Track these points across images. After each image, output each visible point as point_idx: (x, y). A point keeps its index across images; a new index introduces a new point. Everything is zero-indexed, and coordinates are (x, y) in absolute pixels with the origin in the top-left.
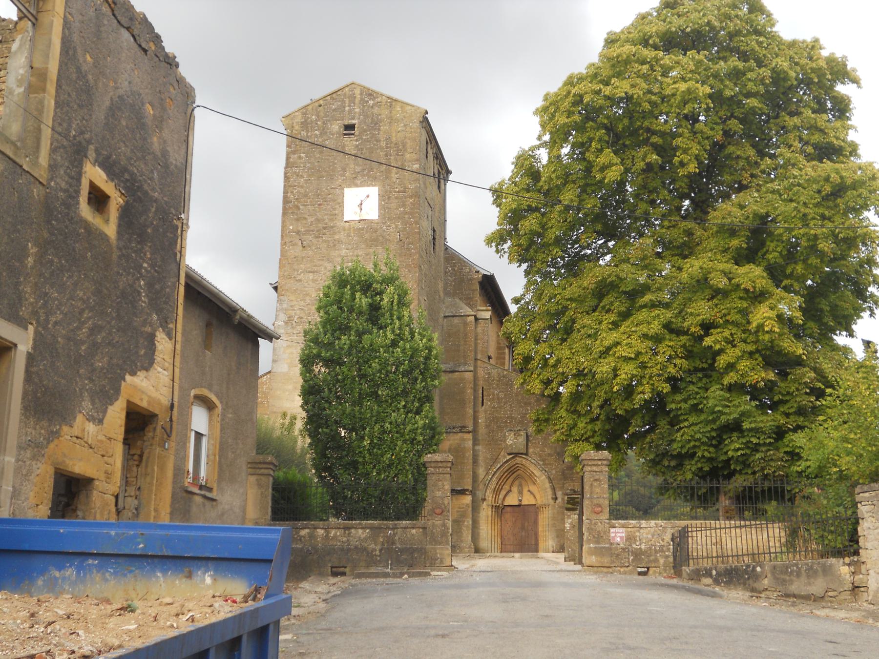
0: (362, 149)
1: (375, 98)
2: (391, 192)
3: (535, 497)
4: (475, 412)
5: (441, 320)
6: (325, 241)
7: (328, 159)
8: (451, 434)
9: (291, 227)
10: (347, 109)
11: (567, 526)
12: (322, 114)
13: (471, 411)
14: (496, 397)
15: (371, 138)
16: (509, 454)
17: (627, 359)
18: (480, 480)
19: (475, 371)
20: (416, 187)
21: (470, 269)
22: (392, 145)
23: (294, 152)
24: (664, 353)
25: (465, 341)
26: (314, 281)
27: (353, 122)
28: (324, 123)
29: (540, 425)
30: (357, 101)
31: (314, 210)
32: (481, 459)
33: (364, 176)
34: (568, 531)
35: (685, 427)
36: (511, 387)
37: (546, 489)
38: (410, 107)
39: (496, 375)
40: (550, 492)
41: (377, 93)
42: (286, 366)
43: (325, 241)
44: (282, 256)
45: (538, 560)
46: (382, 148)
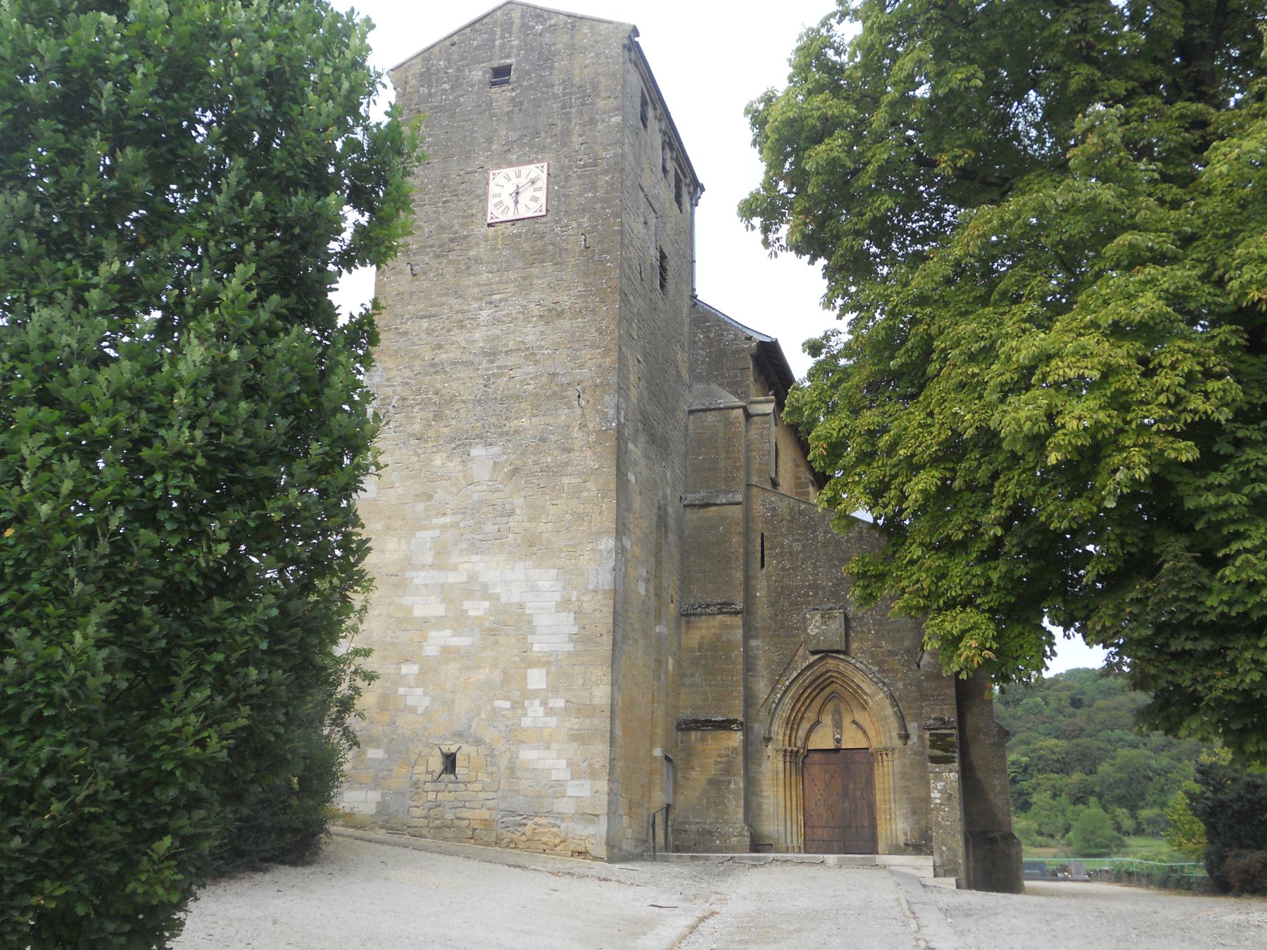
0: (521, 103)
1: (545, 20)
2: (570, 168)
3: (865, 732)
4: (748, 578)
5: (681, 415)
6: (451, 262)
7: (462, 127)
8: (703, 618)
10: (498, 43)
11: (935, 795)
12: (455, 57)
13: (739, 575)
15: (538, 83)
16: (814, 653)
17: (1074, 387)
18: (761, 702)
19: (747, 503)
20: (615, 154)
21: (736, 335)
22: (575, 89)
24: (1173, 367)
25: (728, 452)
26: (429, 332)
27: (508, 61)
28: (458, 70)
29: (868, 586)
30: (515, 29)
31: (435, 212)
32: (761, 663)
33: (522, 146)
34: (938, 808)
35: (1246, 550)
36: (813, 532)
37: (887, 718)
38: (606, 25)
39: (786, 511)
40: (894, 724)
41: (549, 11)
43: (451, 262)
45: (872, 872)
46: (556, 97)
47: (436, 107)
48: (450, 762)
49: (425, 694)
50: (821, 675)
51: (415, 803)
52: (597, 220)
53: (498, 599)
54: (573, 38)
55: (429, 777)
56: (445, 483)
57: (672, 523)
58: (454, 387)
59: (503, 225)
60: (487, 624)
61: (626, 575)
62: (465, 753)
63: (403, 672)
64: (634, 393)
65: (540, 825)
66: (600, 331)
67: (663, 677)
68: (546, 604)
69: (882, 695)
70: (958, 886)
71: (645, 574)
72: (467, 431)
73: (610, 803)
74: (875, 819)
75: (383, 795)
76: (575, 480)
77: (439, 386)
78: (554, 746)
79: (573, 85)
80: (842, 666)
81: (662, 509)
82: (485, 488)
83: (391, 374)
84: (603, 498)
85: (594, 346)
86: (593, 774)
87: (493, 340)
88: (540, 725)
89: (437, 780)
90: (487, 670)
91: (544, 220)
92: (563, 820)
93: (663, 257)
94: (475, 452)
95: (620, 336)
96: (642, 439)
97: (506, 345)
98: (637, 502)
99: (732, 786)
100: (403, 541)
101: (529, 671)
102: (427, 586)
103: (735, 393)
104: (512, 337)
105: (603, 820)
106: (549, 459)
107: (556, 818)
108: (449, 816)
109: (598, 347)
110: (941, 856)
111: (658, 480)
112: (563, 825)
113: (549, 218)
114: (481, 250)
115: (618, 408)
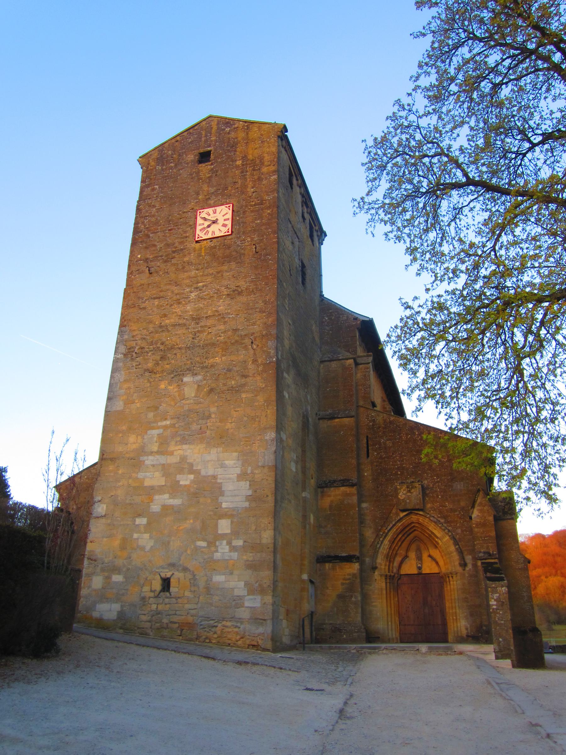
0: (217, 171)
1: (232, 125)
2: (246, 206)
3: (437, 563)
6: (174, 265)
9: (139, 256)
10: (203, 139)
11: (493, 602)
13: (354, 462)
14: (383, 445)
20: (273, 197)
21: (347, 317)
23: (148, 186)
27: (209, 149)
28: (180, 155)
30: (213, 131)
31: (163, 236)
40: (456, 557)
42: (121, 403)
43: (174, 265)
44: (127, 285)
46: (237, 167)
47: (166, 176)
48: (166, 583)
49: (151, 537)
50: (406, 527)
51: (143, 612)
52: (263, 236)
53: (200, 473)
54: (247, 134)
55: (152, 594)
56: (167, 399)
57: (311, 427)
58: (174, 339)
59: (205, 242)
60: (192, 490)
61: (283, 456)
62: (177, 577)
63: (137, 523)
64: (286, 343)
65: (227, 627)
66: (265, 302)
67: (307, 526)
68: (231, 476)
69: (447, 537)
70: (514, 666)
71: (295, 458)
72: (181, 367)
73: (274, 612)
74: (445, 619)
75: (121, 606)
76: (250, 395)
77: (164, 340)
78: (236, 572)
79: (248, 160)
80: (421, 519)
81: (305, 418)
82: (192, 401)
83: (135, 333)
84: (267, 406)
85: (261, 311)
86: (262, 591)
87: (199, 310)
88: (227, 558)
89: (157, 597)
90: (191, 521)
91: (230, 237)
92: (242, 623)
93: (303, 266)
94: (185, 379)
95: (278, 305)
96: (292, 372)
97: (207, 313)
98: (289, 410)
99: (353, 599)
100: (139, 437)
101: (219, 521)
102: (153, 466)
103: (348, 351)
104: (210, 308)
105: (269, 623)
106: (233, 382)
107: (237, 622)
108: (165, 621)
109: (264, 312)
110: (499, 645)
111: (303, 400)
112: (242, 627)
113: (234, 235)
114: (192, 257)
115: (277, 349)
